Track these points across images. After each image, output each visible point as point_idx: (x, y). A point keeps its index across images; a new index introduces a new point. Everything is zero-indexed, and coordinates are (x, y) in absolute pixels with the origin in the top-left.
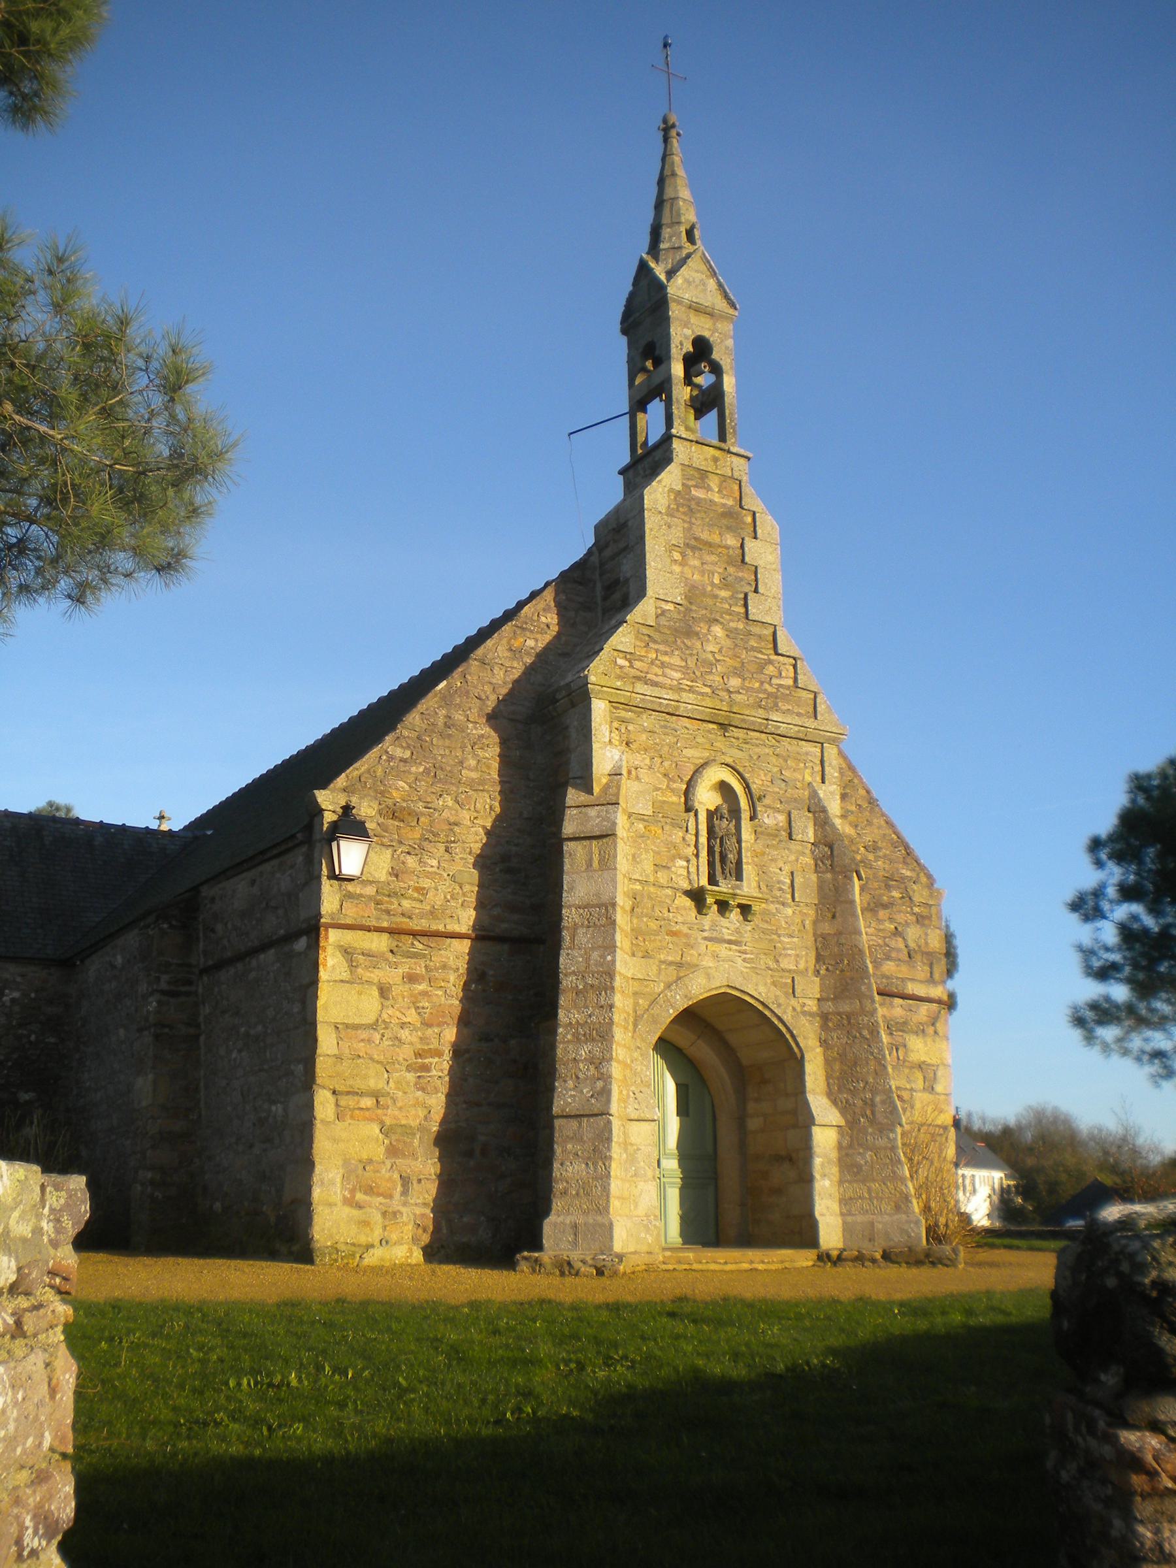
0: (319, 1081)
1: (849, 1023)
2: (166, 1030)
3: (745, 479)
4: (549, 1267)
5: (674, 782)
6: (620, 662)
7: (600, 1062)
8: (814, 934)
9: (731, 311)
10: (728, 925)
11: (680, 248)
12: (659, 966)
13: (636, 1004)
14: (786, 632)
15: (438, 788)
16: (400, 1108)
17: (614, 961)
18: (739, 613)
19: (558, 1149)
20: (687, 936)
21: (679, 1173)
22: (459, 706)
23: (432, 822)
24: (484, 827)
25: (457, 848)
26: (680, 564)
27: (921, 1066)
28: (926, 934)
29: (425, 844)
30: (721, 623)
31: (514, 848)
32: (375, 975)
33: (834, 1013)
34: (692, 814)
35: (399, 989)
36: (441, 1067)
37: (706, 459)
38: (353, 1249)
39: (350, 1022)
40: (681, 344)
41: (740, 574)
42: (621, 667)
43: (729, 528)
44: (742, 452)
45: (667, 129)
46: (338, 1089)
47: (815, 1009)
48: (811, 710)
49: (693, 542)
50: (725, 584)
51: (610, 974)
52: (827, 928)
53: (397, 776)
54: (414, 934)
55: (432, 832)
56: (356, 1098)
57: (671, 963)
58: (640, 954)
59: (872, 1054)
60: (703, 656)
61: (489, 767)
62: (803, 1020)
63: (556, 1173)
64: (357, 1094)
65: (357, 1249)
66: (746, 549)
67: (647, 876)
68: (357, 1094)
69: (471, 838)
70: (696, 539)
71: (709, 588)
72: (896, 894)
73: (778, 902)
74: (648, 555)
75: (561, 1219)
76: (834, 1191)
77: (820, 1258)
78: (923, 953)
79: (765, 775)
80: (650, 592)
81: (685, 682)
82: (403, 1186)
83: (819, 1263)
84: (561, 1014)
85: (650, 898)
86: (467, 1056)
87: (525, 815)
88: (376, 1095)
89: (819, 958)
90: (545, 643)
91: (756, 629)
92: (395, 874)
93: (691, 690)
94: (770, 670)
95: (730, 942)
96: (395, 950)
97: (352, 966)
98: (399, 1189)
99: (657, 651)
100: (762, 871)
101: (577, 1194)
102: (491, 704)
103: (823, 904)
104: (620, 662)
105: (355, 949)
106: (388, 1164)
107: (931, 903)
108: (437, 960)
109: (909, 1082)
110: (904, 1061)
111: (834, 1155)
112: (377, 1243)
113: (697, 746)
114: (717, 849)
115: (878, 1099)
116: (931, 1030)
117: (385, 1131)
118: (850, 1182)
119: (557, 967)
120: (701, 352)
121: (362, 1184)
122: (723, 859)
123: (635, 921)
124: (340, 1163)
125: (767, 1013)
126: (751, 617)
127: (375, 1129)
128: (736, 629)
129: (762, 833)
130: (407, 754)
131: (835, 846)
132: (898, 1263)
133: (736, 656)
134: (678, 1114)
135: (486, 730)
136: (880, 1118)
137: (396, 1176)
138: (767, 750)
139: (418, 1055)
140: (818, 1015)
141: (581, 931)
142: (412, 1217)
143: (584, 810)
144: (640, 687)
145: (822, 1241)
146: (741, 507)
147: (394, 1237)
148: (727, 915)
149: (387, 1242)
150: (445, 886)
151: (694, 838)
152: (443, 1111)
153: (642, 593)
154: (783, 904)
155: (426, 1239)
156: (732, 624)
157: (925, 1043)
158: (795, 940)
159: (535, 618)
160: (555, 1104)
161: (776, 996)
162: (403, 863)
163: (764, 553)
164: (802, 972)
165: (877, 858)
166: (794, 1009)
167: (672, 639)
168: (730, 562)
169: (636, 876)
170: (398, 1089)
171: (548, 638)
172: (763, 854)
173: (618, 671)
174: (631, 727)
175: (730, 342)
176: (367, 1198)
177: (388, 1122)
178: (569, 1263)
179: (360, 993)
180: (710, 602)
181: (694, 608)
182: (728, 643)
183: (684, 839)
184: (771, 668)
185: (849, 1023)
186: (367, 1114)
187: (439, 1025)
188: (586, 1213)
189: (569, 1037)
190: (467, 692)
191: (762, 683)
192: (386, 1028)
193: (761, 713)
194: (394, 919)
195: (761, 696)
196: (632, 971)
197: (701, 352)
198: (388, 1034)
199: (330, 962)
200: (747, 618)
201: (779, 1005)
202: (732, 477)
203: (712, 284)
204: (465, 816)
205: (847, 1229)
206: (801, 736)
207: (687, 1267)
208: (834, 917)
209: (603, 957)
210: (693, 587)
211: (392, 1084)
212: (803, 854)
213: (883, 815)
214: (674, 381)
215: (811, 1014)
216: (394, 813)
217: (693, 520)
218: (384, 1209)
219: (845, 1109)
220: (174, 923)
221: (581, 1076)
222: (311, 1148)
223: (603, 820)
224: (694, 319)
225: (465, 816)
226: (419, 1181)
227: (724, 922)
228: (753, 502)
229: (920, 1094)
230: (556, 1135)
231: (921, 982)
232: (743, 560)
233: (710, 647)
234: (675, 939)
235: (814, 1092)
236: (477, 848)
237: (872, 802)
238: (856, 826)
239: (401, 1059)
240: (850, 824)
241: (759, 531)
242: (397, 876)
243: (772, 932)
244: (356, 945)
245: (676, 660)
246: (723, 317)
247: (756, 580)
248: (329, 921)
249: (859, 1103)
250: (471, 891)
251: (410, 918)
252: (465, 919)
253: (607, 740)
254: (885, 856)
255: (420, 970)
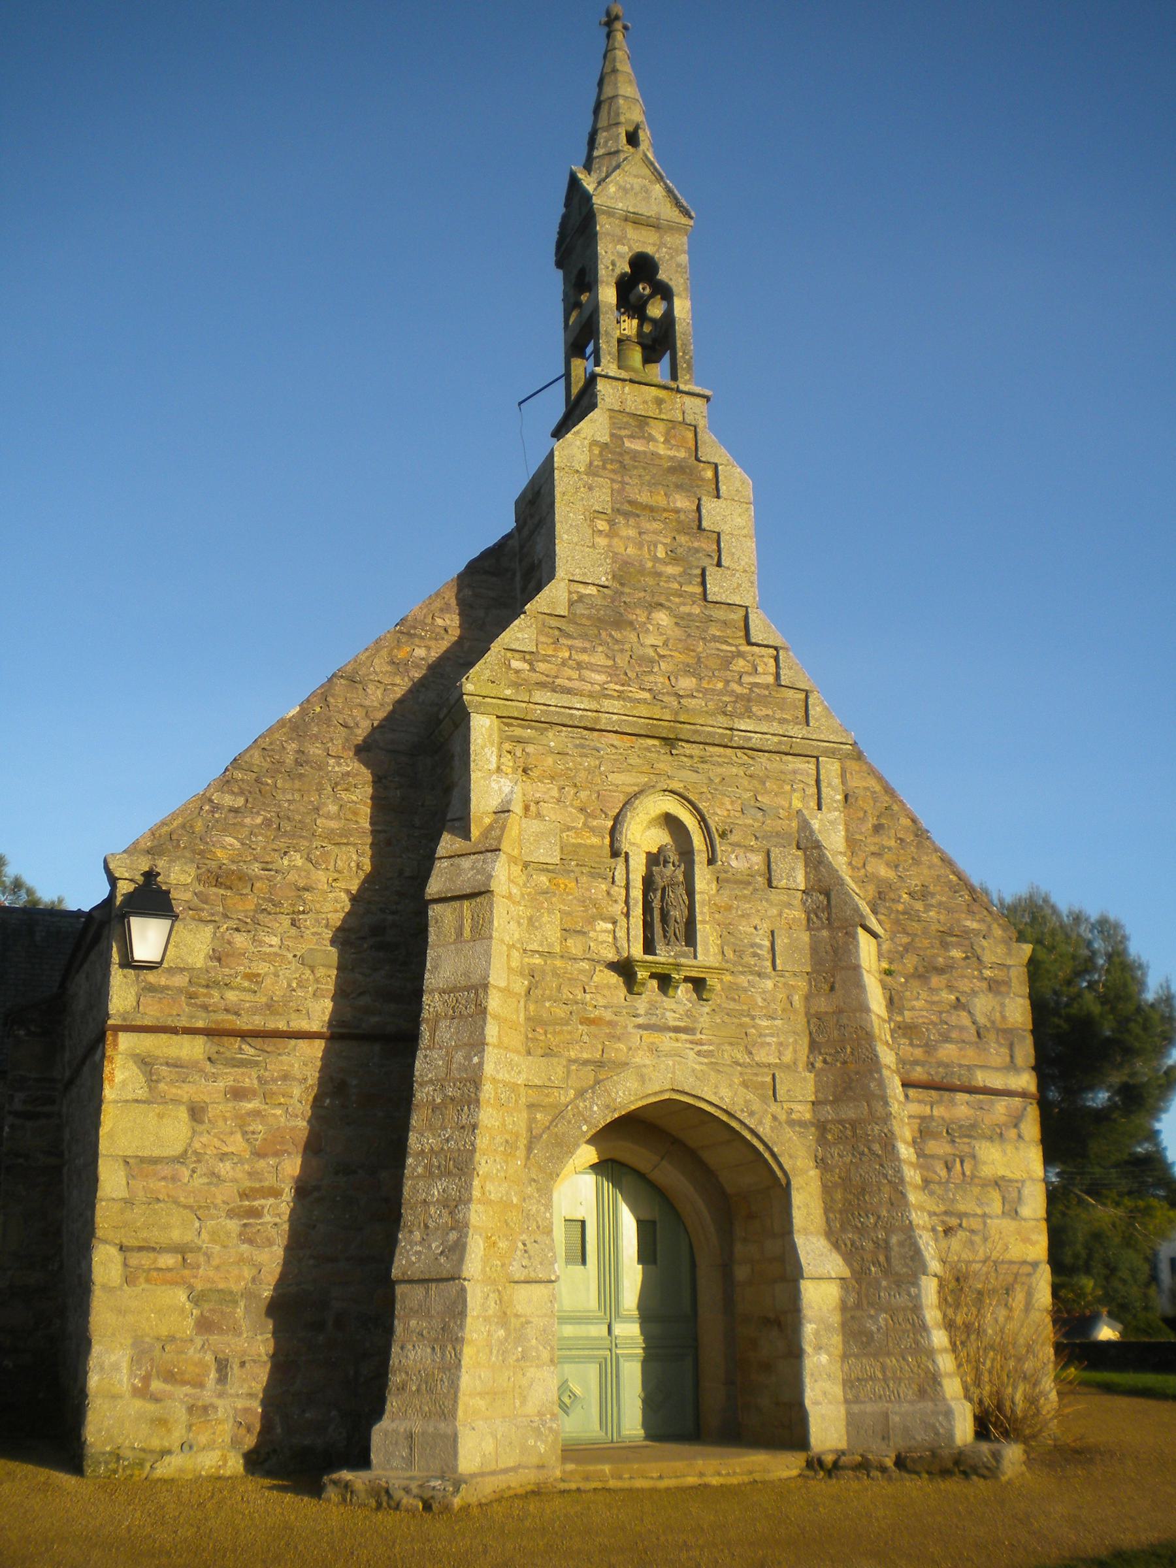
0: (99, 1233)
1: (854, 1134)
2: (21, 1161)
3: (702, 423)
4: (363, 1495)
5: (595, 818)
6: (516, 664)
7: (456, 1204)
8: (807, 1014)
9: (684, 220)
10: (674, 1006)
11: (617, 152)
12: (567, 1067)
13: (532, 1120)
14: (762, 616)
15: (281, 844)
16: (217, 1268)
17: (481, 1064)
18: (693, 595)
19: (399, 1327)
20: (611, 1024)
21: (640, 1340)
22: (316, 737)
23: (272, 888)
24: (348, 892)
25: (307, 921)
26: (607, 536)
27: (998, 1183)
28: (1003, 1005)
29: (261, 917)
30: (668, 608)
31: (390, 918)
32: (185, 1092)
33: (833, 1122)
34: (621, 859)
35: (219, 1109)
36: (278, 1213)
37: (645, 402)
38: (142, 1455)
39: (146, 1153)
40: (613, 264)
41: (696, 544)
42: (517, 672)
43: (679, 487)
44: (697, 389)
45: (610, 21)
46: (125, 1242)
47: (808, 1116)
48: (801, 714)
49: (627, 507)
50: (674, 557)
51: (475, 1081)
52: (822, 1004)
53: (224, 830)
54: (244, 1035)
55: (271, 901)
56: (152, 1255)
57: (586, 1062)
58: (540, 1052)
59: (885, 1176)
60: (641, 651)
61: (355, 813)
62: (789, 1133)
63: (394, 1361)
64: (154, 1249)
65: (148, 1456)
66: (704, 511)
67: (550, 945)
68: (154, 1249)
69: (328, 907)
70: (630, 502)
71: (649, 564)
72: (957, 953)
73: (752, 973)
74: (558, 526)
75: (394, 1425)
76: (837, 1370)
77: (809, 1464)
78: (998, 1030)
79: (732, 803)
80: (560, 573)
81: (612, 686)
82: (219, 1370)
83: (811, 1473)
84: (412, 1138)
85: (555, 974)
86: (316, 1194)
87: (407, 874)
88: (182, 1250)
89: (813, 1046)
90: (441, 651)
91: (719, 613)
92: (217, 957)
93: (621, 696)
94: (740, 664)
95: (677, 1030)
96: (214, 1056)
97: (152, 1080)
98: (213, 1375)
99: (570, 648)
100: (727, 932)
101: (418, 1390)
102: (361, 734)
103: (818, 972)
104: (516, 664)
105: (158, 1057)
106: (199, 1341)
107: (1009, 962)
108: (275, 1067)
109: (980, 1203)
110: (973, 1177)
111: (835, 1319)
112: (176, 1447)
113: (631, 768)
114: (656, 904)
115: (894, 1240)
116: (1012, 1133)
117: (197, 1299)
118: (856, 1356)
119: (412, 1074)
120: (643, 267)
121: (157, 1367)
122: (666, 910)
123: (532, 1007)
124: (130, 1341)
125: (734, 1124)
126: (710, 598)
127: (182, 1296)
128: (689, 614)
129: (727, 881)
130: (240, 802)
131: (833, 894)
132: (918, 1473)
133: (689, 649)
134: (641, 1260)
135: (353, 766)
136: (898, 1266)
137: (209, 1357)
138: (734, 770)
139: (244, 1195)
140: (813, 1124)
141: (443, 1024)
142: (232, 1413)
143: (456, 860)
144: (539, 696)
145: (813, 1441)
146: (697, 459)
147: (203, 1439)
148: (671, 992)
149: (191, 1447)
150: (290, 971)
151: (623, 892)
152: (279, 1269)
153: (551, 576)
154: (759, 975)
155: (250, 1441)
156: (682, 609)
157: (1004, 1152)
158: (778, 1022)
159: (429, 620)
160: (395, 1264)
161: (747, 1102)
162: (229, 943)
163: (732, 516)
164: (788, 1067)
165: (928, 907)
166: (775, 1118)
167: (593, 632)
168: (682, 528)
169: (535, 946)
170: (213, 1241)
171: (444, 645)
172: (729, 908)
173: (512, 676)
174: (530, 749)
175: (684, 259)
176: (168, 1387)
177: (199, 1286)
178: (387, 1492)
179: (160, 1116)
180: (650, 581)
181: (627, 590)
182: (678, 633)
183: (608, 893)
184: (741, 662)
185: (854, 1134)
186: (169, 1275)
187: (276, 1154)
188: (427, 1417)
189: (420, 1170)
190: (329, 719)
191: (727, 682)
192: (199, 1161)
193: (722, 720)
194: (214, 1016)
195: (726, 699)
196: (524, 1076)
197: (643, 267)
198: (202, 1169)
199: (119, 1076)
200: (705, 599)
201: (752, 1114)
202: (684, 422)
203: (658, 190)
204: (321, 878)
205: (853, 1422)
206: (783, 748)
207: (599, 1485)
208: (832, 989)
209: (468, 1058)
210: (626, 563)
211: (204, 1235)
212: (789, 905)
213: (937, 850)
214: (602, 309)
215: (802, 1124)
216: (218, 878)
217: (627, 479)
218: (191, 1401)
219: (850, 1254)
220: (33, 1029)
221: (431, 1224)
222: (88, 1322)
223: (478, 872)
224: (631, 232)
225: (321, 878)
226: (243, 1364)
227: (668, 1003)
228: (714, 450)
229: (997, 1221)
230: (398, 1306)
231: (997, 1069)
232: (700, 527)
233: (650, 640)
234: (593, 1028)
235: (806, 1232)
236: (337, 919)
237: (921, 834)
238: (897, 866)
239: (218, 1201)
240: (888, 865)
241: (723, 489)
242: (219, 960)
243: (742, 1014)
244: (158, 1053)
245: (599, 659)
246: (673, 228)
247: (719, 550)
248: (119, 1023)
249: (868, 1245)
250: (328, 977)
251: (237, 1014)
252: (318, 1012)
253: (493, 766)
254: (940, 904)
255: (249, 1080)
